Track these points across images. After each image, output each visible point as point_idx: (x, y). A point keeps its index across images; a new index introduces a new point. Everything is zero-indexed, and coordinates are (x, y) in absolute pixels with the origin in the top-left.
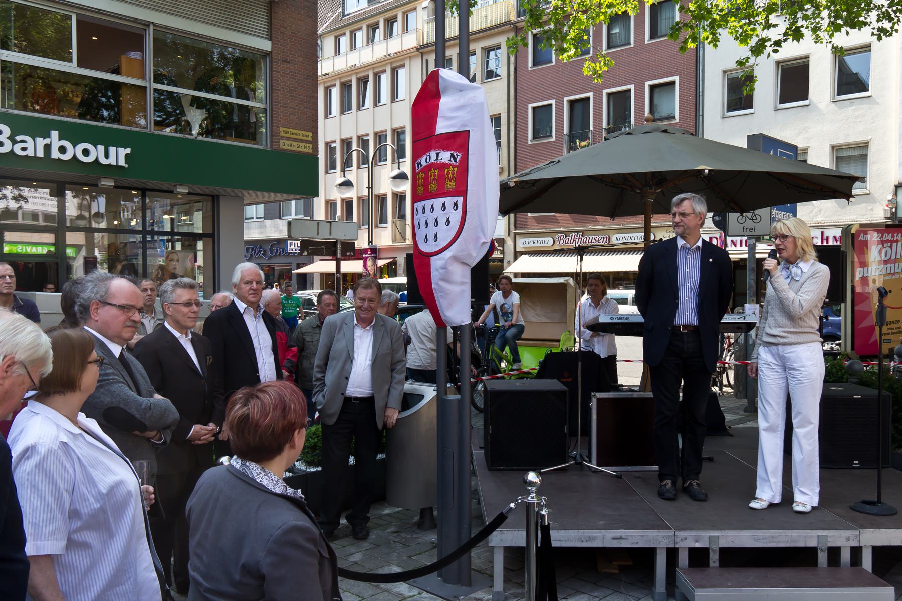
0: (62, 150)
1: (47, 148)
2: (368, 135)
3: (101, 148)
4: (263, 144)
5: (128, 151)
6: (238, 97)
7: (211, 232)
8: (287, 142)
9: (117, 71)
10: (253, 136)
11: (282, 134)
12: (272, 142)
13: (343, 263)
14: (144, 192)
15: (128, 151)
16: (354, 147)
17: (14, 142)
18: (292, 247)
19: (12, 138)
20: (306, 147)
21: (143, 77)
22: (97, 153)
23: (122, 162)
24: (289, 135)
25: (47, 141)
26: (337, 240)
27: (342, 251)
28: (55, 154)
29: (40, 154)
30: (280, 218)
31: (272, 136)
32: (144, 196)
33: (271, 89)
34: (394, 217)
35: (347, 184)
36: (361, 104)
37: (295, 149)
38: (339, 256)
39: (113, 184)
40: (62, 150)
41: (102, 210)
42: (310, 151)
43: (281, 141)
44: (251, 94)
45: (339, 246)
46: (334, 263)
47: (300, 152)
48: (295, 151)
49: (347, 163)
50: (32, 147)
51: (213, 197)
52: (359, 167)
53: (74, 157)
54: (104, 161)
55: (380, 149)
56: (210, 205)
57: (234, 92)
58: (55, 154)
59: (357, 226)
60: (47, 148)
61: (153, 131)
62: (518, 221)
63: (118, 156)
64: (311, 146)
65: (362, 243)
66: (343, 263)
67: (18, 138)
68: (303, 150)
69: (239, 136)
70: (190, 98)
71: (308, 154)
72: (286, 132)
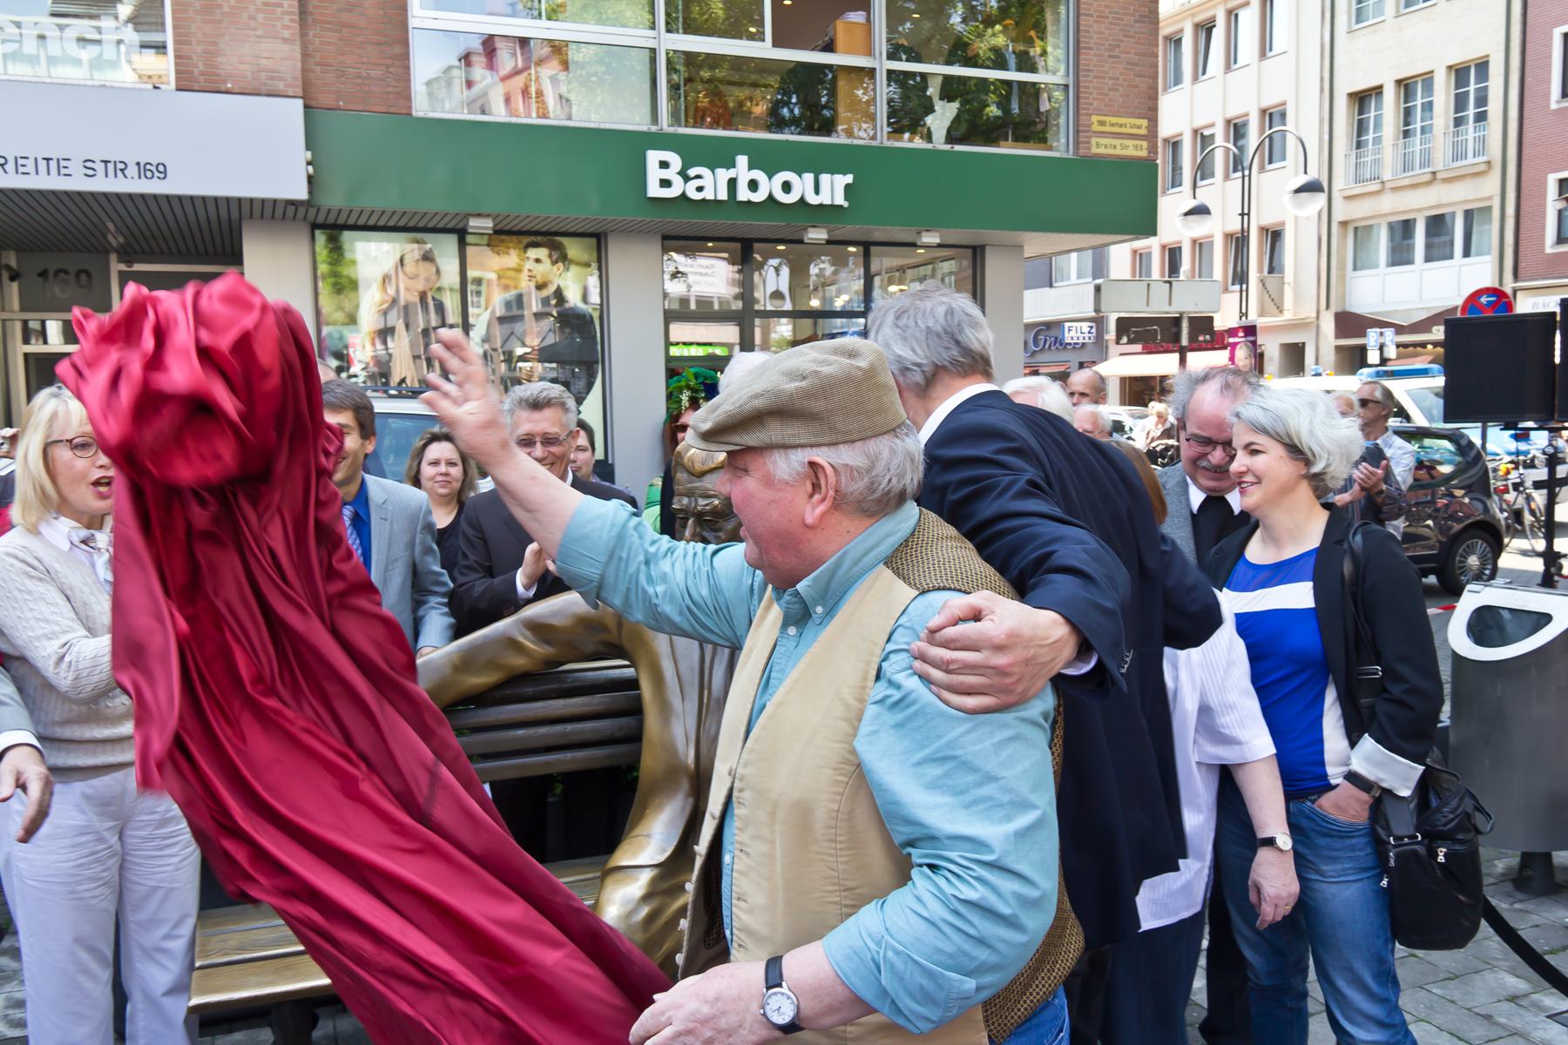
0: (753, 185)
1: (732, 183)
2: (1213, 125)
3: (809, 177)
4: (1060, 147)
5: (849, 178)
6: (1020, 69)
9: (829, 47)
10: (1042, 140)
11: (1096, 127)
12: (1077, 143)
14: (599, 239)
15: (849, 178)
17: (687, 179)
18: (1073, 333)
20: (1136, 147)
21: (869, 52)
22: (803, 186)
23: (840, 200)
24: (1107, 129)
25: (732, 173)
26: (1181, 314)
28: (744, 194)
29: (723, 195)
30: (1051, 286)
33: (1078, 49)
34: (1260, 270)
35: (1201, 211)
36: (1201, 68)
37: (1119, 152)
38: (1185, 342)
39: (825, 236)
40: (753, 185)
42: (1144, 153)
43: (1094, 141)
44: (1041, 63)
46: (1176, 356)
47: (1125, 158)
48: (1118, 156)
49: (1203, 170)
50: (711, 184)
52: (1227, 177)
53: (771, 197)
54: (813, 199)
55: (1270, 137)
56: (966, 263)
57: (1012, 61)
58: (744, 194)
60: (732, 183)
62: (1522, 264)
63: (833, 189)
64: (1145, 144)
65: (1225, 319)
66: (1191, 356)
67: (692, 172)
68: (1131, 152)
70: (939, 80)
71: (1140, 159)
72: (1102, 123)
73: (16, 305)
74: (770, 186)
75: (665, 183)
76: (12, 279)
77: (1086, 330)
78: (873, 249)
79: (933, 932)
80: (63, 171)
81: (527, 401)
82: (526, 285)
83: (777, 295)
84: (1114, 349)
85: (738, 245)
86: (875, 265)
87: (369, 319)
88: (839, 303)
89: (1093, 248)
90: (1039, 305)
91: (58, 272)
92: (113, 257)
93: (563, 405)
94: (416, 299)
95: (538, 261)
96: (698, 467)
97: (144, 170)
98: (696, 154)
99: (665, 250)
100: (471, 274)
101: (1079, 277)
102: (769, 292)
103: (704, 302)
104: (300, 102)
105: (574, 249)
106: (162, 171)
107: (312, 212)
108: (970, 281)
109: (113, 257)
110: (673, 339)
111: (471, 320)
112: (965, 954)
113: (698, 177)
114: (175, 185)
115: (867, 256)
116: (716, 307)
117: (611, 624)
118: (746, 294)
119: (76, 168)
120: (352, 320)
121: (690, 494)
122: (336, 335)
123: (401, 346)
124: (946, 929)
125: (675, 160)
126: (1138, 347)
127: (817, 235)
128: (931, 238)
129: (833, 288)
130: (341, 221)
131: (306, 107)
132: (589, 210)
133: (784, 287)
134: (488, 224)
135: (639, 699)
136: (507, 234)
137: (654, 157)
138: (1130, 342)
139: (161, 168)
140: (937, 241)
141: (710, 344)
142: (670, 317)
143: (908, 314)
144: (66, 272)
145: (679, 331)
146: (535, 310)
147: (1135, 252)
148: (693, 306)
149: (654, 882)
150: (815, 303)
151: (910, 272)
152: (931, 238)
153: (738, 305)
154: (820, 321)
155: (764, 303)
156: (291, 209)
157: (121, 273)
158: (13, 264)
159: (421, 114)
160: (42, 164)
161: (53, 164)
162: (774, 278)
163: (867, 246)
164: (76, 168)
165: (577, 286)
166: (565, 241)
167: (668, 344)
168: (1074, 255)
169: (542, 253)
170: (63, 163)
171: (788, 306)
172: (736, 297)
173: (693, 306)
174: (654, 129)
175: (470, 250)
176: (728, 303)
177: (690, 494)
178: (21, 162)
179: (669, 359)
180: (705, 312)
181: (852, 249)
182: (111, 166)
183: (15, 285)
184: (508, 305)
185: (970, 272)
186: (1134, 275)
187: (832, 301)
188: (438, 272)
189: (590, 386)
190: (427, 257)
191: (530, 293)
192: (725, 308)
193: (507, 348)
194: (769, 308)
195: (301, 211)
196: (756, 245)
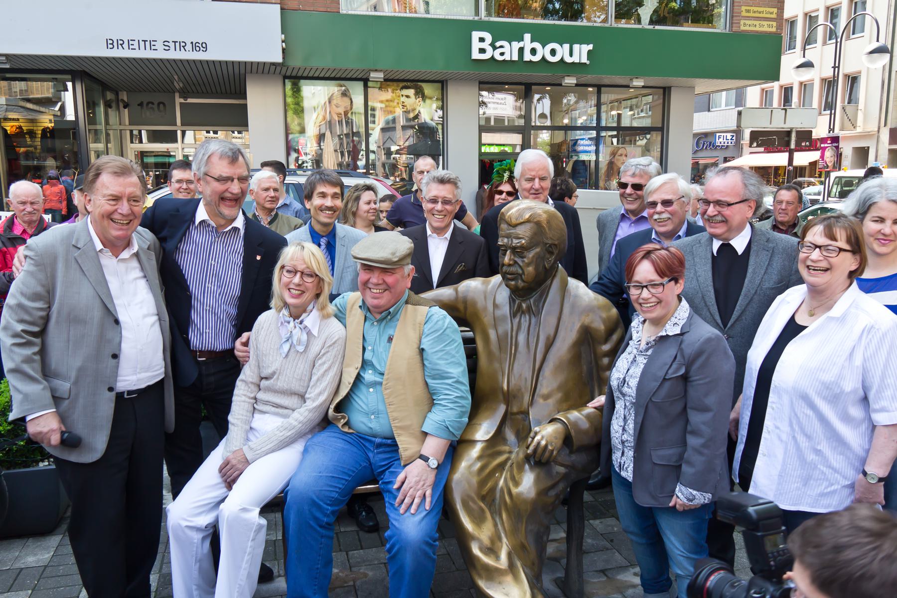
1: (521, 50)
3: (567, 46)
4: (720, 27)
5: (591, 47)
8: (748, 22)
11: (744, 14)
12: (732, 24)
13: (797, 155)
14: (442, 84)
15: (591, 47)
16: (821, 21)
17: (495, 48)
18: (721, 140)
19: (493, 45)
22: (563, 52)
23: (584, 60)
25: (521, 44)
27: (796, 141)
28: (528, 57)
29: (515, 57)
31: (732, 17)
32: (599, 93)
35: (808, 65)
37: (757, 29)
38: (793, 146)
40: (533, 51)
41: (547, 112)
42: (774, 30)
43: (742, 22)
45: (794, 136)
46: (786, 155)
47: (762, 32)
48: (757, 32)
49: (809, 41)
51: (664, 89)
52: (825, 43)
53: (543, 58)
54: (568, 60)
58: (528, 57)
59: (817, 112)
60: (521, 50)
61: (615, 25)
63: (581, 53)
64: (774, 24)
66: (797, 155)
67: (498, 44)
68: (766, 29)
69: (695, 21)
71: (771, 33)
72: (748, 11)
73: (127, 123)
74: (543, 52)
75: (482, 51)
76: (125, 107)
78: (603, 89)
80: (153, 47)
91: (148, 103)
92: (177, 95)
95: (408, 97)
96: (514, 221)
97: (195, 46)
98: (501, 33)
104: (279, 6)
105: (428, 89)
106: (204, 47)
107: (284, 69)
109: (177, 95)
111: (370, 132)
113: (501, 47)
114: (213, 54)
117: (461, 306)
119: (159, 45)
121: (508, 236)
125: (488, 37)
127: (570, 81)
128: (638, 83)
130: (300, 74)
131: (282, 9)
132: (438, 68)
134: (381, 75)
136: (390, 81)
137: (476, 35)
139: (204, 45)
140: (642, 84)
144: (153, 103)
145: (487, 138)
148: (492, 123)
149: (484, 450)
152: (638, 83)
156: (273, 68)
157: (181, 103)
158: (125, 99)
159: (344, 12)
160: (142, 44)
161: (148, 44)
163: (599, 87)
164: (159, 45)
166: (424, 85)
167: (481, 144)
169: (411, 92)
170: (153, 43)
173: (492, 123)
174: (476, 18)
177: (508, 236)
178: (131, 42)
179: (481, 154)
181: (590, 89)
182: (177, 44)
183: (126, 110)
187: (576, 119)
192: (511, 124)
195: (278, 69)
196: (533, 87)
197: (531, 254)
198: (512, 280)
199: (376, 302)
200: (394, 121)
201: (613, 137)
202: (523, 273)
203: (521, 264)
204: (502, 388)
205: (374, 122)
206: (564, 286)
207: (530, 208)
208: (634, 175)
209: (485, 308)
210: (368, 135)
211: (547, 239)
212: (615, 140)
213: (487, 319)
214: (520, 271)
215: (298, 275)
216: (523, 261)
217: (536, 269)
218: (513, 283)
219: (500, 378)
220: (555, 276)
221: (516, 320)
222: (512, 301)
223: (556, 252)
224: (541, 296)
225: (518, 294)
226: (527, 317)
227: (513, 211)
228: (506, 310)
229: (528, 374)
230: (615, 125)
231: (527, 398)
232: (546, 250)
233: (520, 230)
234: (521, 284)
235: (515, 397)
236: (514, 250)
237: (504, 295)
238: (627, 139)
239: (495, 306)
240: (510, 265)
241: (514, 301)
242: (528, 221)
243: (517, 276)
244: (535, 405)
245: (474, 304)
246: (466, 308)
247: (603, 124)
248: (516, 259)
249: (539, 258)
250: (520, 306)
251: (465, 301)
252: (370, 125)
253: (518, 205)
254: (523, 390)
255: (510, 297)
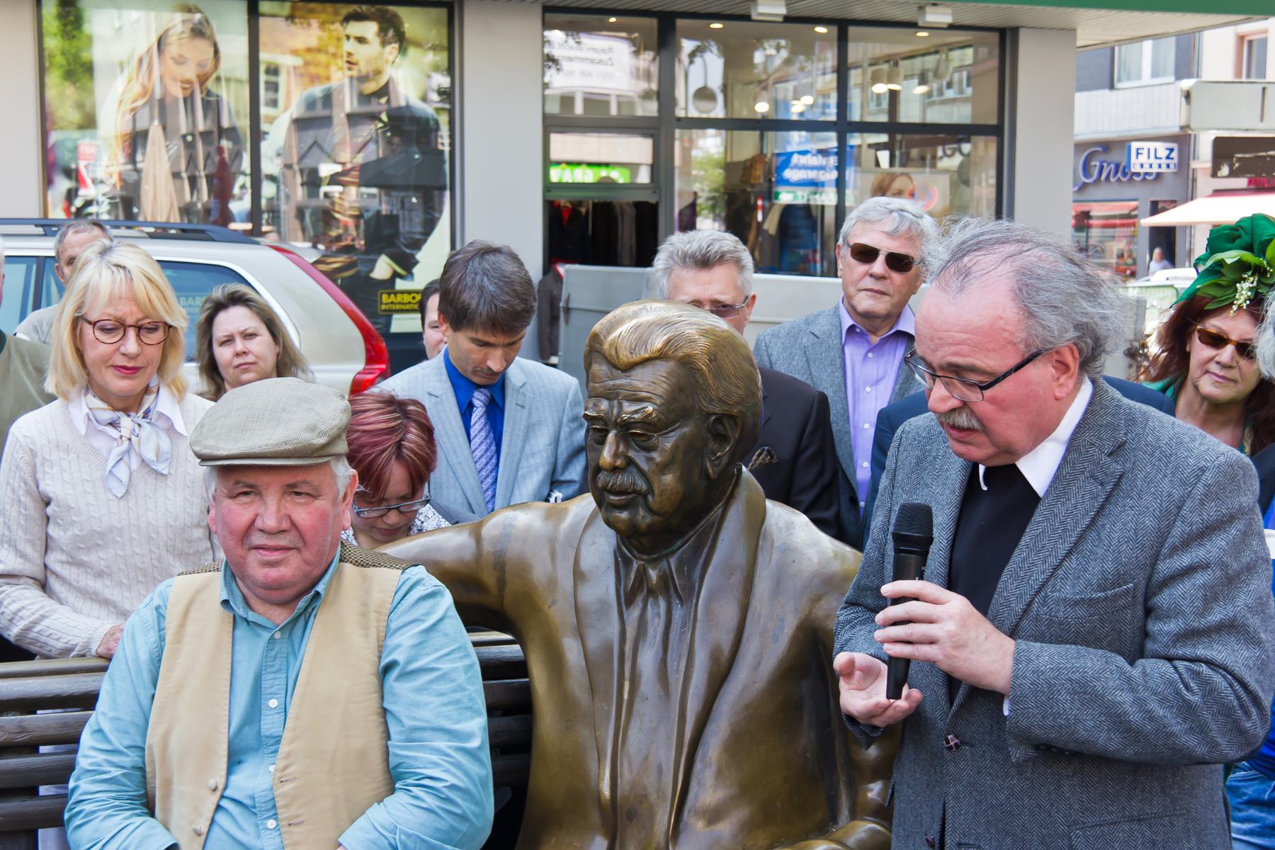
7: (993, 121)
18: (1143, 158)
30: (1112, 87)
39: (782, 11)
77: (1163, 153)
78: (852, 30)
79: (431, 817)
81: (693, 256)
82: (339, 78)
83: (704, 94)
84: (1205, 183)
85: (653, 22)
86: (856, 51)
87: (113, 121)
88: (797, 108)
89: (1179, 35)
90: (1096, 115)
93: (738, 262)
94: (178, 92)
95: (361, 40)
96: (625, 356)
99: (547, 26)
100: (265, 56)
101: (1155, 74)
102: (693, 87)
103: (595, 102)
108: (994, 77)
110: (554, 155)
111: (264, 127)
112: (454, 829)
115: (843, 40)
116: (614, 111)
117: (489, 578)
118: (665, 95)
120: (89, 123)
121: (611, 395)
122: (70, 145)
123: (159, 161)
124: (441, 813)
126: (1242, 182)
129: (790, 86)
133: (715, 82)
135: (527, 690)
138: (1233, 174)
141: (607, 165)
142: (551, 125)
143: (202, 173)
145: (563, 145)
146: (348, 109)
147: (1241, 38)
148: (579, 109)
150: (762, 108)
151: (903, 64)
153: (651, 109)
154: (770, 135)
155: (687, 107)
162: (702, 69)
163: (843, 26)
165: (412, 79)
167: (548, 162)
168: (1148, 45)
169: (370, 29)
171: (718, 112)
172: (646, 96)
173: (579, 109)
175: (264, 23)
176: (631, 104)
179: (548, 187)
180: (599, 118)
181: (821, 30)
184: (311, 104)
185: (995, 62)
186: (1239, 74)
187: (787, 107)
188: (216, 52)
189: (429, 226)
190: (199, 32)
191: (341, 90)
192: (626, 112)
193: (309, 162)
194: (694, 113)
196: (680, 23)
197: (668, 442)
198: (621, 507)
199: (273, 573)
200: (328, 99)
201: (878, 147)
202: (650, 490)
203: (644, 466)
204: (598, 793)
205: (274, 103)
206: (756, 523)
207: (667, 324)
208: (891, 235)
209: (553, 582)
210: (257, 136)
211: (711, 401)
212: (884, 156)
213: (559, 611)
214: (641, 485)
215: (132, 333)
216: (650, 460)
217: (684, 477)
218: (624, 515)
219: (593, 766)
220: (732, 496)
221: (633, 614)
222: (622, 563)
223: (734, 435)
224: (697, 549)
225: (638, 543)
226: (662, 603)
227: (624, 329)
228: (602, 587)
229: (666, 756)
230: (884, 118)
231: (663, 819)
232: (709, 430)
233: (642, 380)
234: (643, 518)
235: (631, 815)
236: (626, 430)
237: (600, 546)
238: (915, 152)
239: (579, 575)
240: (614, 470)
241: (628, 562)
242: (661, 356)
243: (633, 498)
244: (683, 838)
245: (524, 569)
246: (502, 582)
247: (855, 115)
248: (631, 454)
249: (690, 454)
250: (642, 576)
251: (500, 565)
252: (264, 111)
253: (635, 315)
254: (653, 797)
255: (618, 553)
